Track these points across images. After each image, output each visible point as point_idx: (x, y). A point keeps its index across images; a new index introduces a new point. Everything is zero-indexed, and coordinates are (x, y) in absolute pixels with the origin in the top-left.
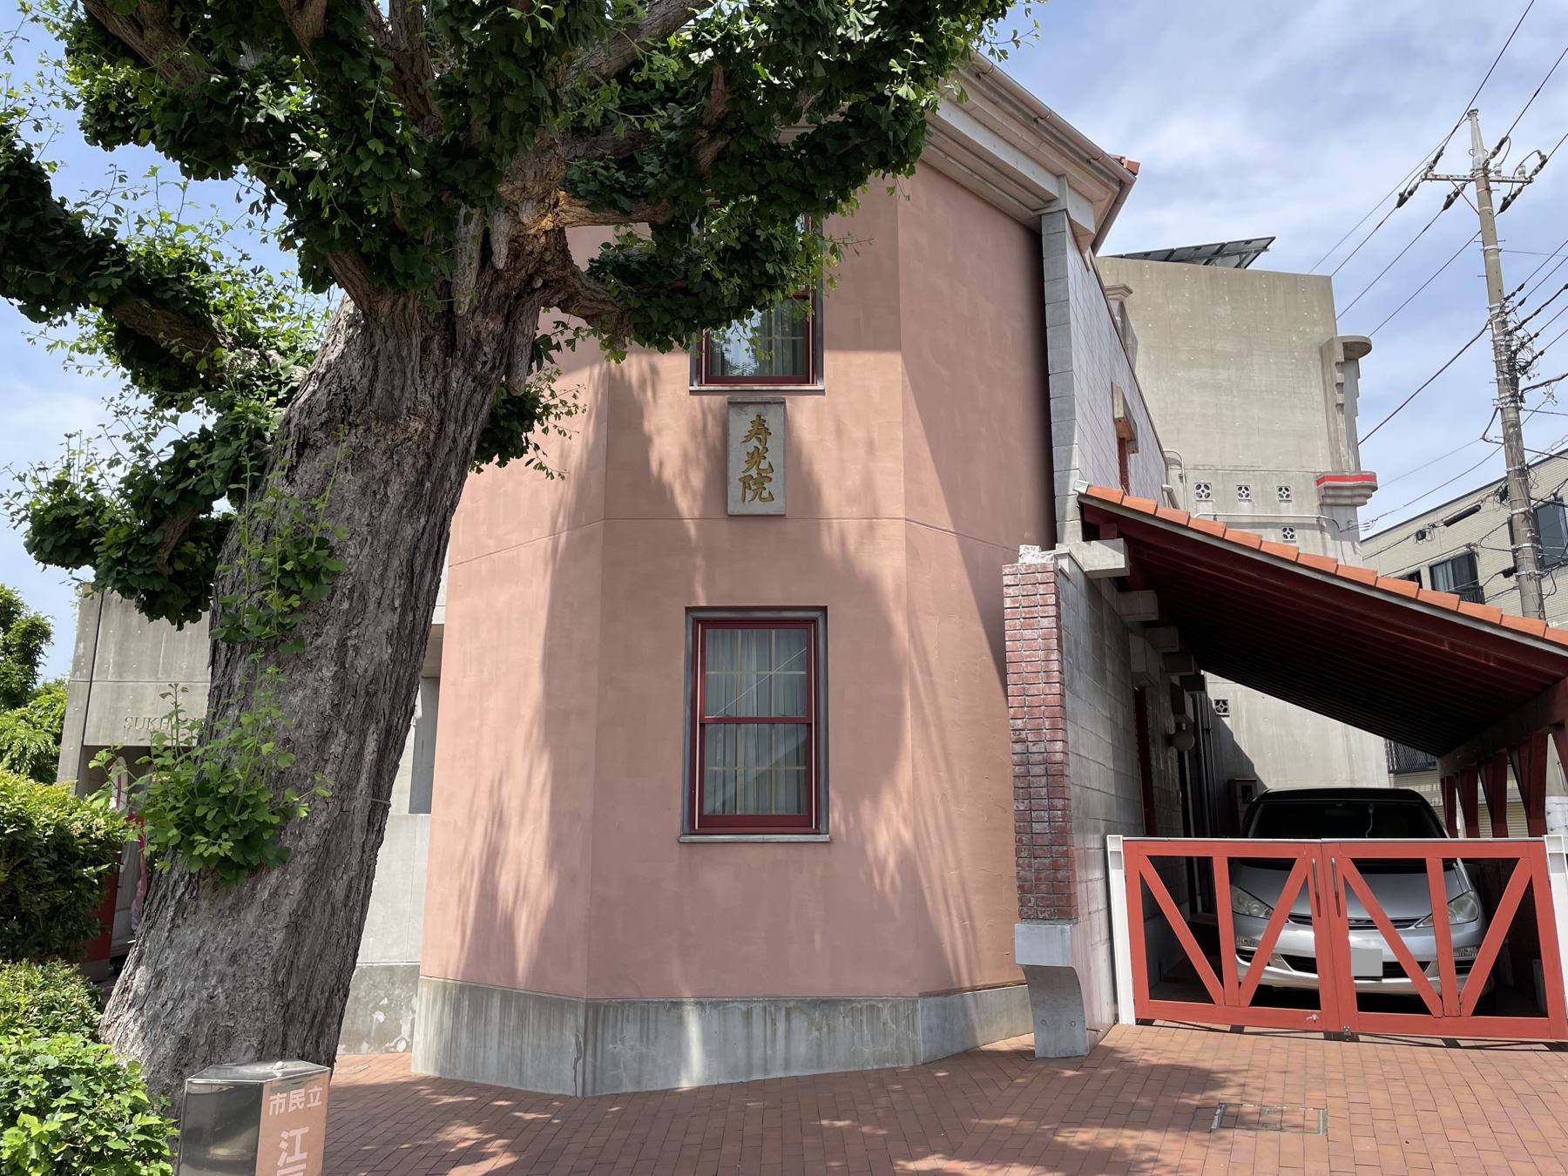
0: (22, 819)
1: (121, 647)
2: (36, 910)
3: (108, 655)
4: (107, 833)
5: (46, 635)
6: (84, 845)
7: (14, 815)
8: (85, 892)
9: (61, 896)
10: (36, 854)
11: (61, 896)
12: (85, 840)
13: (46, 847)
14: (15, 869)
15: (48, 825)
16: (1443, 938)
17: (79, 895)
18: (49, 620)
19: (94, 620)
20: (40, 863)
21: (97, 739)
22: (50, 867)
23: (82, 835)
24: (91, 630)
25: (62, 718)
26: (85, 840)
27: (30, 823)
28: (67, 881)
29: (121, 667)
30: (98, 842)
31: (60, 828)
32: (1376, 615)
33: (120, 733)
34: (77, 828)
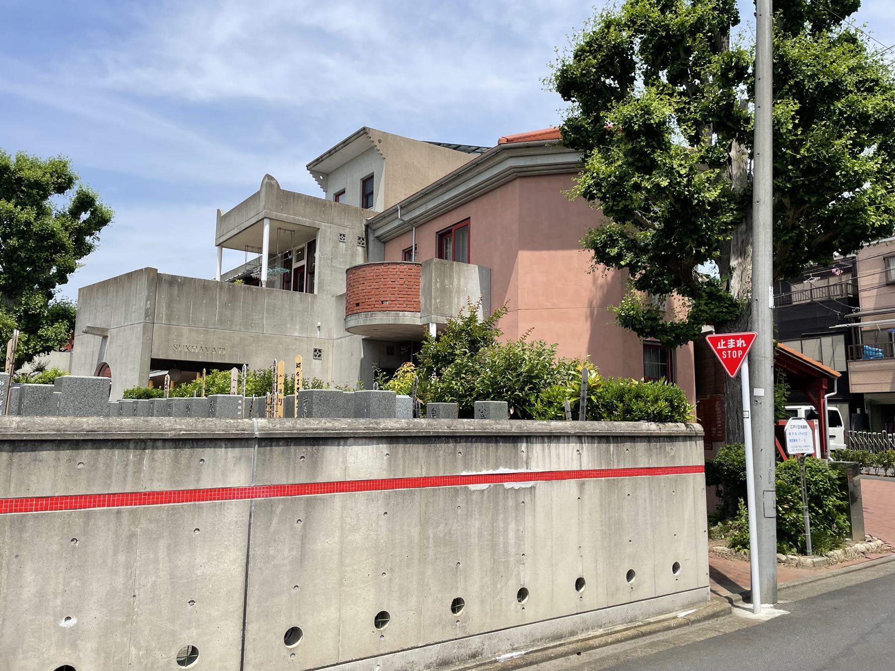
1: (169, 306)
29: (170, 317)
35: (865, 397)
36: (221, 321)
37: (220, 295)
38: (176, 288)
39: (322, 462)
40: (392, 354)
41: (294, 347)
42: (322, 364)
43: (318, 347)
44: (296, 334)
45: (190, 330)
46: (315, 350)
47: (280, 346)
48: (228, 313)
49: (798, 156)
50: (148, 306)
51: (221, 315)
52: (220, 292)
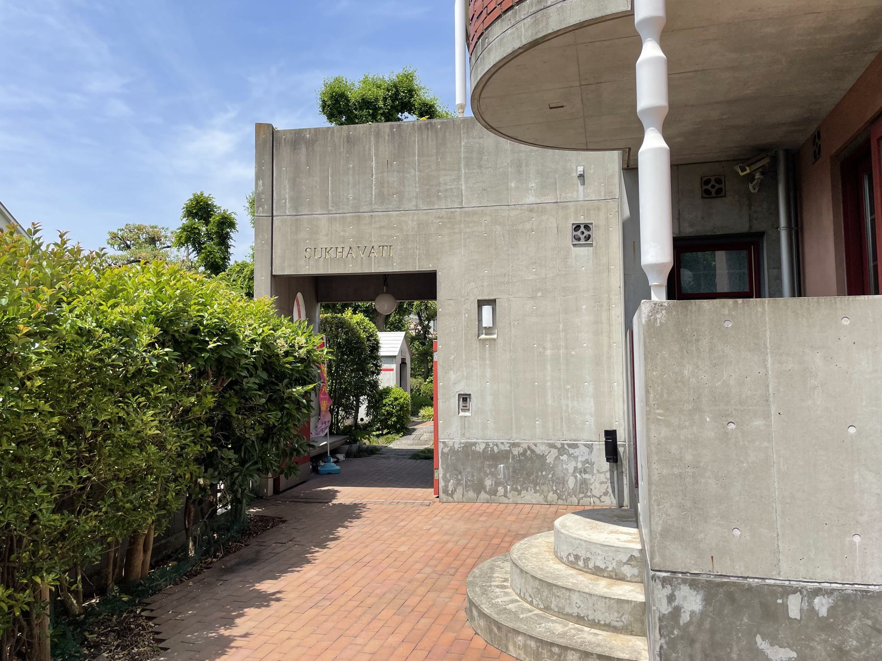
0: (224, 331)
1: (295, 184)
2: (251, 436)
3: (284, 191)
4: (309, 352)
5: (232, 225)
6: (290, 363)
7: (216, 327)
8: (294, 413)
9: (273, 417)
10: (244, 373)
11: (273, 417)
12: (291, 359)
13: (255, 366)
14: (225, 390)
15: (253, 341)
16: (325, 399)
17: (290, 415)
18: (233, 215)
19: (268, 158)
20: (250, 383)
21: (283, 269)
22: (261, 387)
23: (287, 354)
24: (267, 168)
25: (251, 279)
26: (291, 359)
27: (235, 337)
28: (277, 401)
29: (297, 202)
30: (302, 360)
31: (265, 345)
32: (871, 264)
33: (302, 262)
34: (282, 346)
35: (688, 231)
36: (382, 198)
37: (377, 149)
38: (304, 150)
39: (221, 591)
40: (720, 193)
41: (528, 226)
42: (595, 253)
43: (582, 220)
44: (531, 199)
45: (331, 221)
46: (577, 227)
47: (498, 228)
48: (393, 178)
49: (215, 448)
50: (260, 189)
51: (381, 184)
52: (377, 142)
